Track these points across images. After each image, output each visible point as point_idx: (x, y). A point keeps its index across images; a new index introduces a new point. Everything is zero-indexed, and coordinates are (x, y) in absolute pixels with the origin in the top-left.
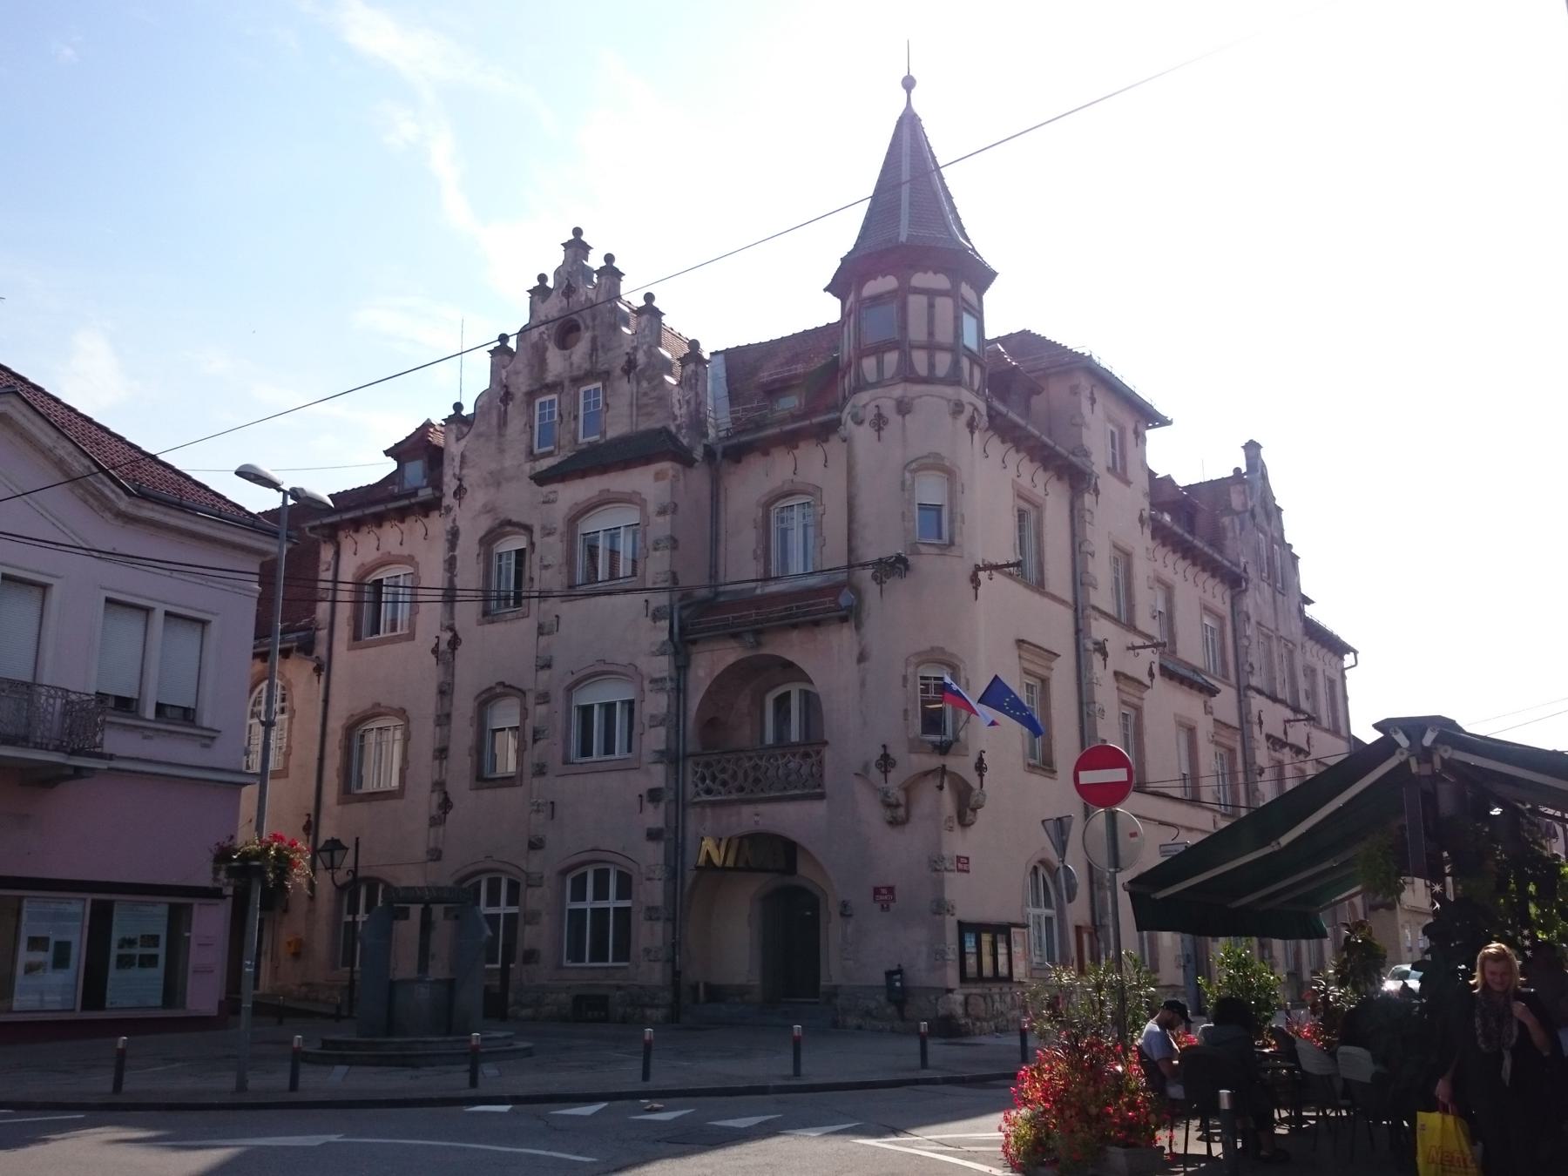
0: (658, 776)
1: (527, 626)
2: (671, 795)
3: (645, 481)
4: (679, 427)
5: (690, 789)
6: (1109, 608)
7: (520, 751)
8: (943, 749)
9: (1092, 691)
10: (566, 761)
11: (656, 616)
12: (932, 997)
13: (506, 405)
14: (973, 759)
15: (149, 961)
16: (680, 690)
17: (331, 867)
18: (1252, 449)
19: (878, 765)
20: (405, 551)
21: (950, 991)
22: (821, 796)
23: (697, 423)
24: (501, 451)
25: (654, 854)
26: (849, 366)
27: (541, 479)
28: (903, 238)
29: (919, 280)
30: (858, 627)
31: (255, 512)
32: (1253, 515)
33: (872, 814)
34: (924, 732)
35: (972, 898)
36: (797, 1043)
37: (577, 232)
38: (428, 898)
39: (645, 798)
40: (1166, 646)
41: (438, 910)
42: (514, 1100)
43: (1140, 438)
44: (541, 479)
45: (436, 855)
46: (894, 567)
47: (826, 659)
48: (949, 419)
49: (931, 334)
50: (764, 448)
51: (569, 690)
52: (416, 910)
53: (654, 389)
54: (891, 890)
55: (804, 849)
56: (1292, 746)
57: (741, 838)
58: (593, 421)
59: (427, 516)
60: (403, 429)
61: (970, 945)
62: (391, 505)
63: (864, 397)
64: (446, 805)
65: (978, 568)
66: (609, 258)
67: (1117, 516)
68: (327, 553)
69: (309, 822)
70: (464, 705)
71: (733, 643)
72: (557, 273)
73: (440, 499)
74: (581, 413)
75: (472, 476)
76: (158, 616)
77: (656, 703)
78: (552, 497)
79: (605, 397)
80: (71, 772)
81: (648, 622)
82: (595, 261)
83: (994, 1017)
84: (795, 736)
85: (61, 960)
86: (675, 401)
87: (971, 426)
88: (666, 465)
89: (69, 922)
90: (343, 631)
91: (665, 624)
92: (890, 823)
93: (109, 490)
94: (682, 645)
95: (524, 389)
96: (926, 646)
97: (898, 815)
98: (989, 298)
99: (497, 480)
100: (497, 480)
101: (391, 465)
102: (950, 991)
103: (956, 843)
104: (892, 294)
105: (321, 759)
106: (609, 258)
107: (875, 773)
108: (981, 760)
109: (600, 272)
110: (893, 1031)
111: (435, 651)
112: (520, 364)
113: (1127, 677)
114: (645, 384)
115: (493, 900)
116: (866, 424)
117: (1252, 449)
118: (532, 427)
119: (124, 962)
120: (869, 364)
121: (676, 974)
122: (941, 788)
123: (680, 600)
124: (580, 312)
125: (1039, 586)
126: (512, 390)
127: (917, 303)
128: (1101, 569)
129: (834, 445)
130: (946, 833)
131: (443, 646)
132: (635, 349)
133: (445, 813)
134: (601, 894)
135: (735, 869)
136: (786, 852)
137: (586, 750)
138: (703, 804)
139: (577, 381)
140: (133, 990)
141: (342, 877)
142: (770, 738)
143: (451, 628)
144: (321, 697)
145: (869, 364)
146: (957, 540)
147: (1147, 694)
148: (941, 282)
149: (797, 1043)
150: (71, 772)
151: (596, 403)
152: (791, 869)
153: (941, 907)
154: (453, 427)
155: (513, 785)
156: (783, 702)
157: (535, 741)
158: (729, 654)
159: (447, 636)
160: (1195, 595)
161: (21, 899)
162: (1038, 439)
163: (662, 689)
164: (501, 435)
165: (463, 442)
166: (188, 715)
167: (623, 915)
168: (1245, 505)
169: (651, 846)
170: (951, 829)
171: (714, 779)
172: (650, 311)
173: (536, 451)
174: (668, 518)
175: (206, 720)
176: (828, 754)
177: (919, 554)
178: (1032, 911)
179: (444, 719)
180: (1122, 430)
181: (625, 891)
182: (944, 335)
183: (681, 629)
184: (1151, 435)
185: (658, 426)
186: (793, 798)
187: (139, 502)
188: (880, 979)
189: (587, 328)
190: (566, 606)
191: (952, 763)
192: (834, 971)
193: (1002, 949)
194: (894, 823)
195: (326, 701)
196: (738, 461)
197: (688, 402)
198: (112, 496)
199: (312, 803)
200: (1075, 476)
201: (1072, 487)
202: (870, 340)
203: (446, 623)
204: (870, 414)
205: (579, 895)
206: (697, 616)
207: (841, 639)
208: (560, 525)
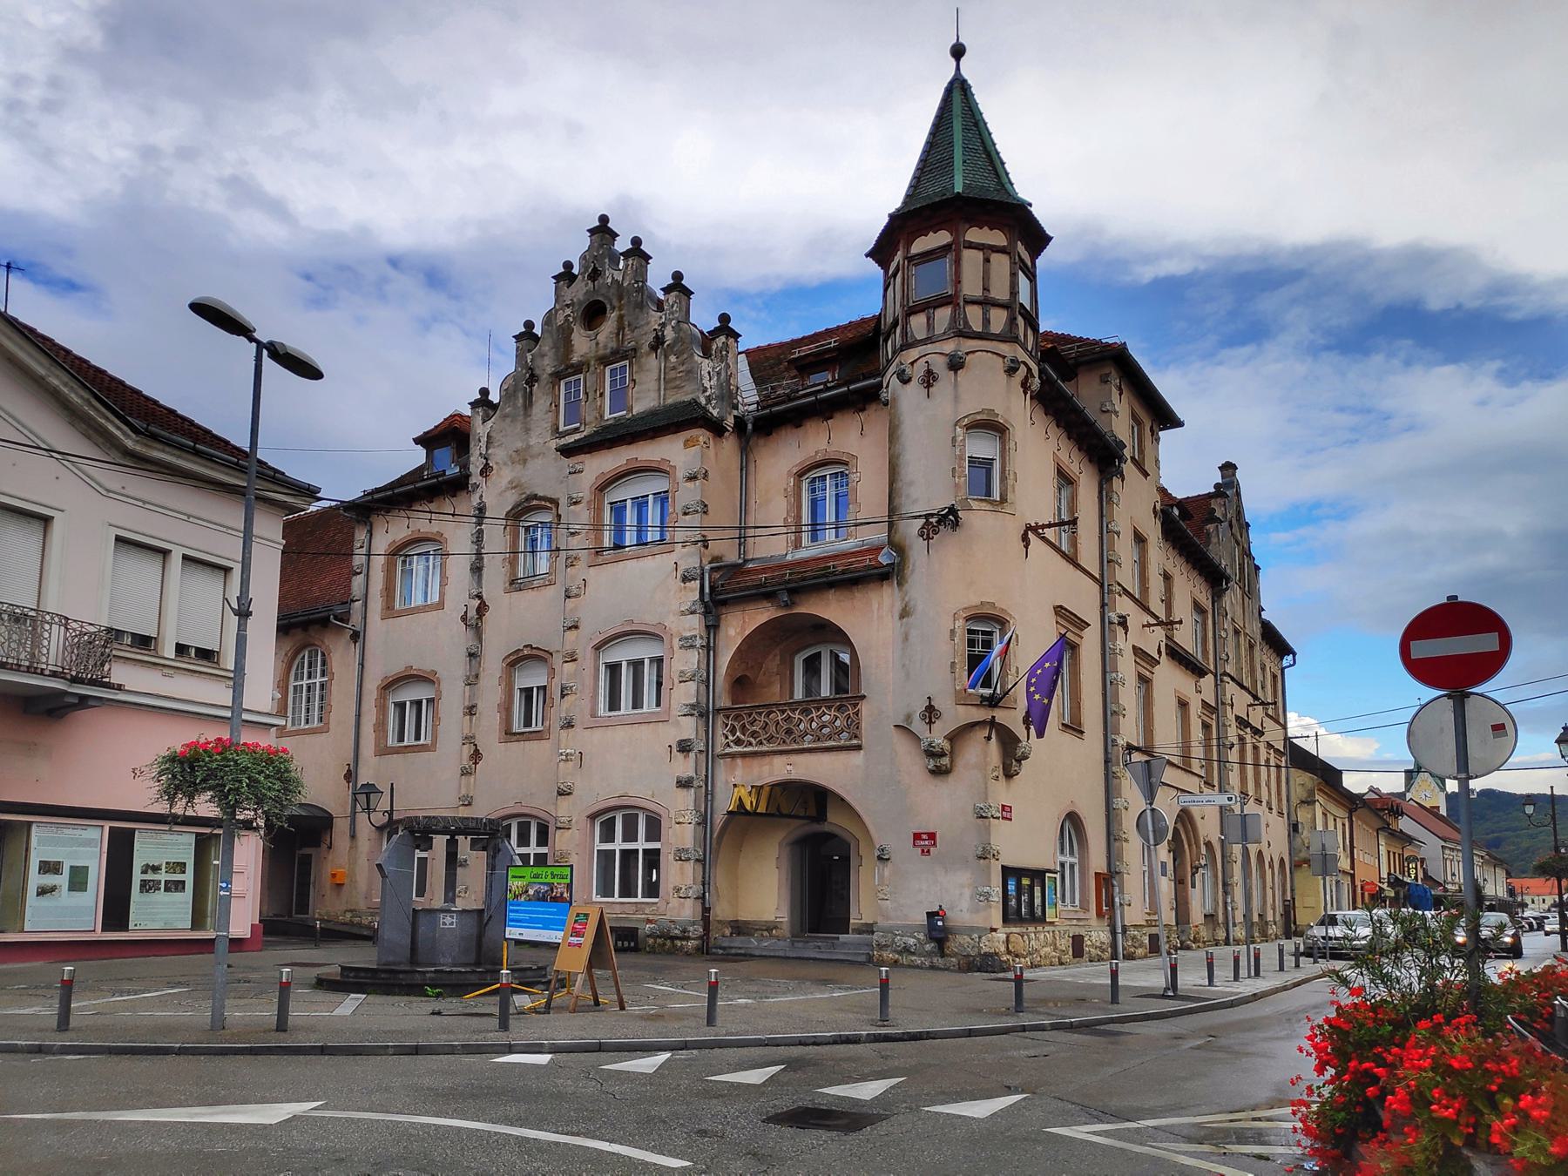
0: (689, 728)
1: (554, 593)
4: (709, 399)
5: (720, 740)
8: (993, 702)
12: (975, 936)
15: (179, 886)
16: (710, 649)
17: (368, 809)
18: (1228, 468)
19: (923, 717)
22: (859, 748)
23: (728, 395)
24: (527, 430)
25: (686, 799)
28: (958, 188)
29: (974, 235)
30: (900, 584)
32: (1231, 526)
33: (912, 764)
38: (455, 829)
39: (674, 750)
40: (1169, 624)
41: (464, 842)
42: (554, 1050)
44: (567, 451)
46: (948, 519)
47: (867, 621)
51: (598, 648)
52: (440, 841)
54: (932, 836)
56: (1252, 728)
57: (773, 786)
60: (432, 420)
61: (1012, 887)
63: (914, 353)
64: (476, 756)
65: (1029, 528)
66: (636, 242)
68: (361, 535)
72: (583, 257)
73: (468, 476)
75: (498, 455)
76: (176, 560)
77: (689, 661)
78: (578, 467)
79: (631, 374)
83: (1030, 953)
85: (78, 880)
87: (1025, 385)
89: (88, 849)
90: (376, 604)
92: (932, 772)
94: (715, 605)
95: (549, 370)
97: (940, 764)
99: (522, 457)
101: (419, 456)
104: (946, 249)
105: (358, 716)
106: (636, 242)
107: (918, 726)
109: (627, 254)
110: (933, 967)
111: (464, 618)
112: (546, 346)
114: (673, 359)
115: (524, 840)
116: (914, 382)
117: (1228, 468)
119: (146, 886)
121: (706, 910)
122: (989, 738)
126: (537, 372)
127: (972, 259)
128: (1125, 549)
131: (472, 613)
132: (663, 325)
134: (630, 835)
137: (614, 704)
140: (159, 913)
141: (379, 818)
143: (479, 596)
145: (918, 323)
146: (1010, 497)
148: (997, 238)
152: (821, 816)
157: (563, 696)
158: (762, 614)
159: (477, 602)
160: (1188, 588)
161: (30, 824)
163: (692, 646)
165: (490, 423)
168: (1225, 515)
169: (682, 792)
176: (865, 707)
179: (472, 680)
183: (711, 588)
185: (687, 398)
188: (923, 920)
189: (613, 308)
191: (1001, 716)
192: (862, 909)
193: (1037, 890)
194: (939, 772)
195: (362, 665)
196: (769, 434)
197: (719, 373)
198: (118, 433)
202: (916, 297)
204: (918, 371)
205: (608, 836)
207: (884, 600)
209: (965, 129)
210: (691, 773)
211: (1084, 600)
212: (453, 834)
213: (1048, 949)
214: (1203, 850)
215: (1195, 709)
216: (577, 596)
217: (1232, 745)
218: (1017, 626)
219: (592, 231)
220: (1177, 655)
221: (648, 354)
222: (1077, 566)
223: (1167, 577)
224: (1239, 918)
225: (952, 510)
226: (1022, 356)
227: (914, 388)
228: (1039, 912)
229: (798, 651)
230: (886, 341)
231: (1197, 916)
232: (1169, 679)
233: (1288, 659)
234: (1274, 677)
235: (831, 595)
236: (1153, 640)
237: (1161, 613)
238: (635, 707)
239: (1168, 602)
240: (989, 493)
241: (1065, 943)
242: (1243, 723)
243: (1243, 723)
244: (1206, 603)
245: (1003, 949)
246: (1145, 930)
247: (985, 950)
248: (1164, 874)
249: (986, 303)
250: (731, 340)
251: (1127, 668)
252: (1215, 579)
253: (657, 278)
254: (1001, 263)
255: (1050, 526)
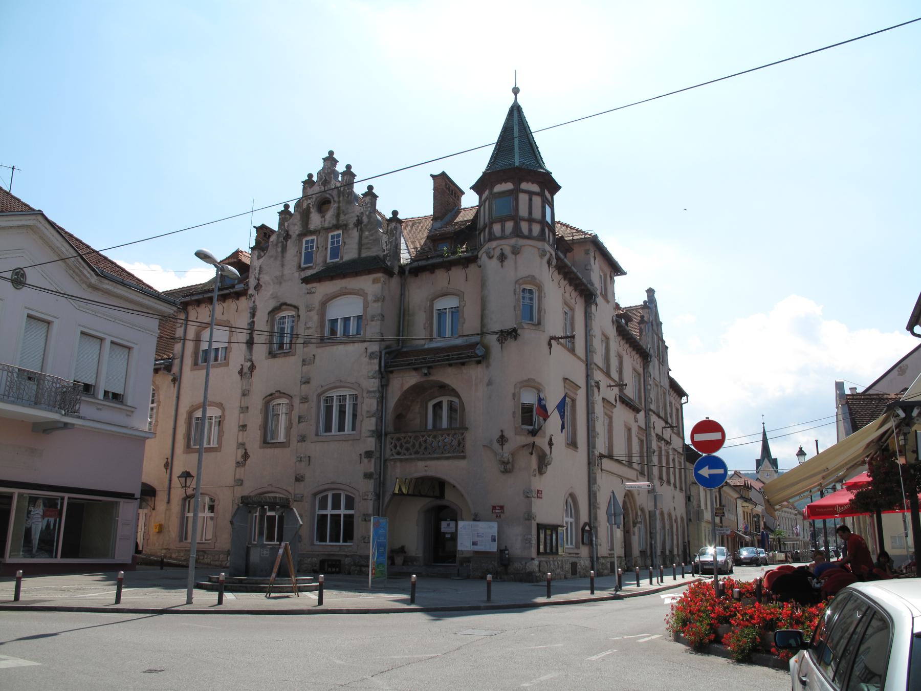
0: (370, 444)
2: (378, 455)
3: (369, 284)
6: (600, 365)
7: (289, 428)
8: (534, 433)
9: (593, 407)
10: (317, 435)
11: (372, 356)
13: (287, 241)
14: (547, 439)
18: (651, 292)
19: (498, 441)
20: (225, 318)
21: (533, 559)
22: (464, 457)
24: (283, 265)
25: (369, 486)
26: (485, 228)
27: (306, 281)
28: (517, 164)
29: (524, 186)
31: (161, 290)
34: (523, 424)
35: (549, 510)
36: (489, 584)
37: (331, 153)
40: (621, 386)
43: (612, 281)
44: (306, 281)
45: (240, 482)
46: (511, 334)
47: (469, 383)
48: (539, 258)
49: (530, 213)
50: (432, 269)
53: (372, 235)
54: (502, 507)
55: (450, 484)
57: (417, 479)
58: (335, 252)
59: (238, 299)
61: (542, 536)
62: (193, 298)
63: (494, 244)
64: (246, 456)
65: (552, 338)
66: (349, 167)
67: (603, 320)
69: (167, 463)
70: (256, 402)
71: (414, 373)
72: (319, 173)
74: (329, 246)
75: (265, 278)
76: (107, 343)
77: (369, 404)
78: (313, 290)
79: (343, 239)
80: (62, 425)
81: (367, 359)
82: (341, 168)
84: (445, 424)
86: (384, 242)
87: (549, 263)
88: (379, 275)
91: (376, 361)
93: (87, 272)
94: (385, 374)
95: (297, 232)
96: (525, 378)
97: (507, 467)
98: (557, 197)
99: (280, 280)
100: (280, 280)
102: (533, 559)
103: (538, 483)
106: (349, 167)
107: (496, 446)
108: (551, 440)
109: (343, 174)
112: (297, 219)
113: (608, 402)
116: (495, 259)
117: (651, 292)
118: (301, 253)
120: (497, 228)
122: (531, 454)
123: (386, 348)
124: (331, 195)
125: (572, 351)
126: (290, 233)
127: (523, 198)
128: (597, 343)
129: (472, 268)
130: (533, 478)
132: (362, 213)
133: (245, 460)
134: (336, 506)
135: (414, 495)
136: (438, 486)
137: (328, 428)
138: (395, 460)
139: (328, 230)
142: (430, 426)
143: (251, 360)
144: (175, 396)
147: (615, 410)
148: (535, 188)
149: (489, 584)
150: (62, 425)
151: (338, 242)
152: (442, 496)
153: (529, 517)
154: (256, 252)
155: (284, 447)
156: (438, 406)
157: (299, 422)
158: (411, 379)
159: (249, 364)
160: (631, 362)
161: (117, 502)
162: (575, 274)
164: (283, 257)
165: (261, 260)
166: (116, 397)
167: (349, 519)
170: (535, 475)
171: (401, 446)
172: (370, 194)
173: (303, 266)
174: (380, 304)
175: (130, 401)
177: (523, 328)
178: (566, 519)
179: (244, 409)
180: (605, 275)
181: (350, 504)
182: (537, 214)
183: (386, 366)
184: (617, 279)
185: (374, 254)
186: (448, 458)
187: (103, 280)
190: (320, 350)
194: (506, 471)
195: (178, 398)
196: (416, 276)
198: (88, 275)
199: (170, 452)
200: (587, 295)
201: (586, 301)
203: (248, 357)
204: (497, 253)
205: (323, 506)
206: (395, 357)
207: (475, 372)
208: (317, 305)
209: (520, 131)
210: (372, 470)
211: (578, 375)
212: (262, 507)
213: (559, 570)
214: (639, 513)
215: (634, 431)
216: (309, 364)
217: (654, 452)
218: (563, 444)
219: (325, 160)
220: (625, 401)
221: (353, 229)
222: (575, 355)
223: (620, 358)
224: (659, 553)
225: (515, 330)
226: (548, 248)
227: (495, 263)
228: (554, 550)
229: (430, 400)
230: (480, 234)
231: (636, 551)
232: (621, 414)
233: (684, 399)
234: (677, 410)
235: (450, 370)
236: (612, 394)
237: (617, 379)
238: (339, 431)
239: (620, 372)
240: (531, 319)
241: (568, 567)
242: (660, 438)
243: (660, 438)
244: (641, 370)
245: (537, 569)
246: (608, 560)
247: (528, 570)
248: (618, 527)
249: (530, 220)
250: (398, 225)
251: (599, 409)
252: (644, 356)
253: (359, 189)
254: (537, 200)
255: (562, 338)
